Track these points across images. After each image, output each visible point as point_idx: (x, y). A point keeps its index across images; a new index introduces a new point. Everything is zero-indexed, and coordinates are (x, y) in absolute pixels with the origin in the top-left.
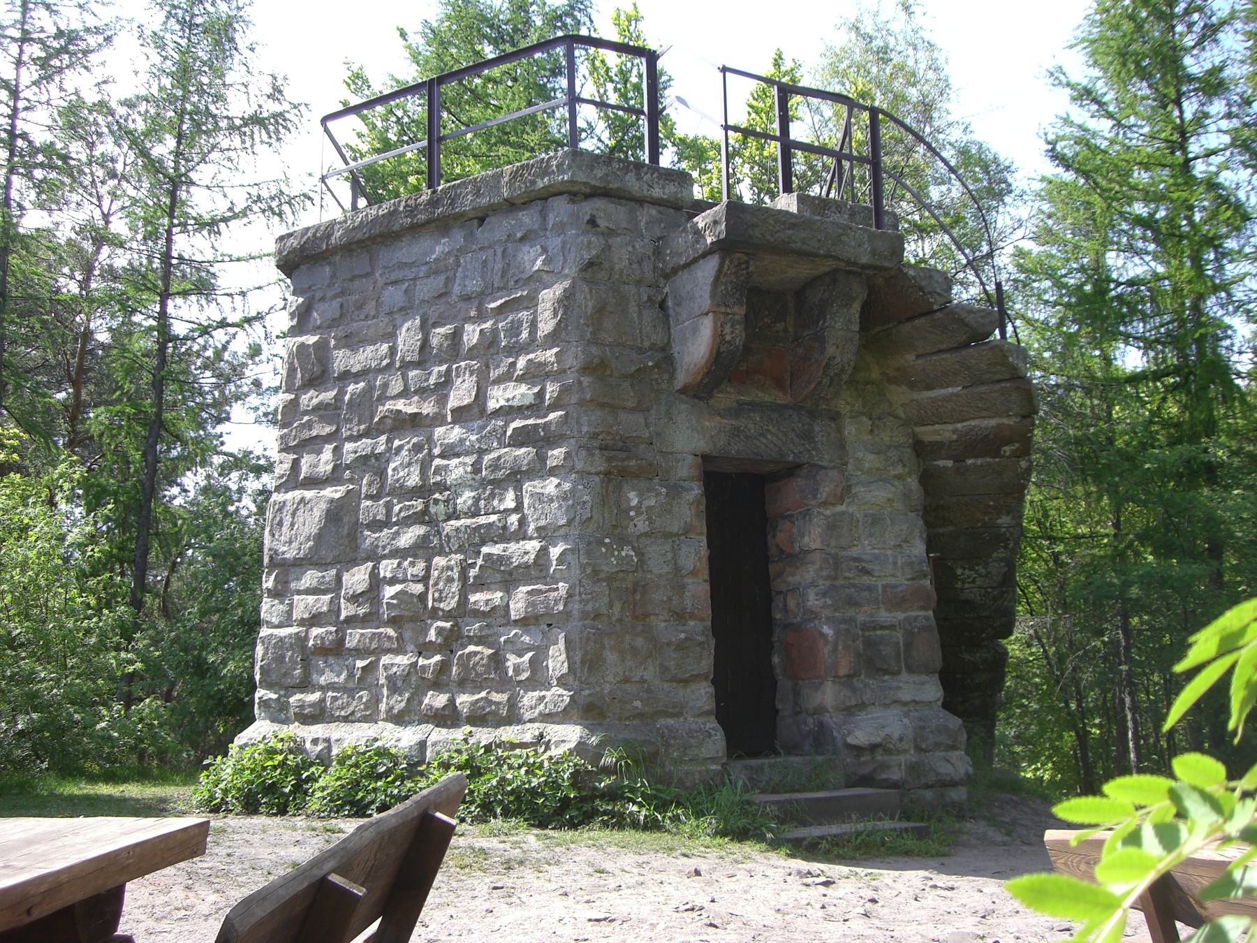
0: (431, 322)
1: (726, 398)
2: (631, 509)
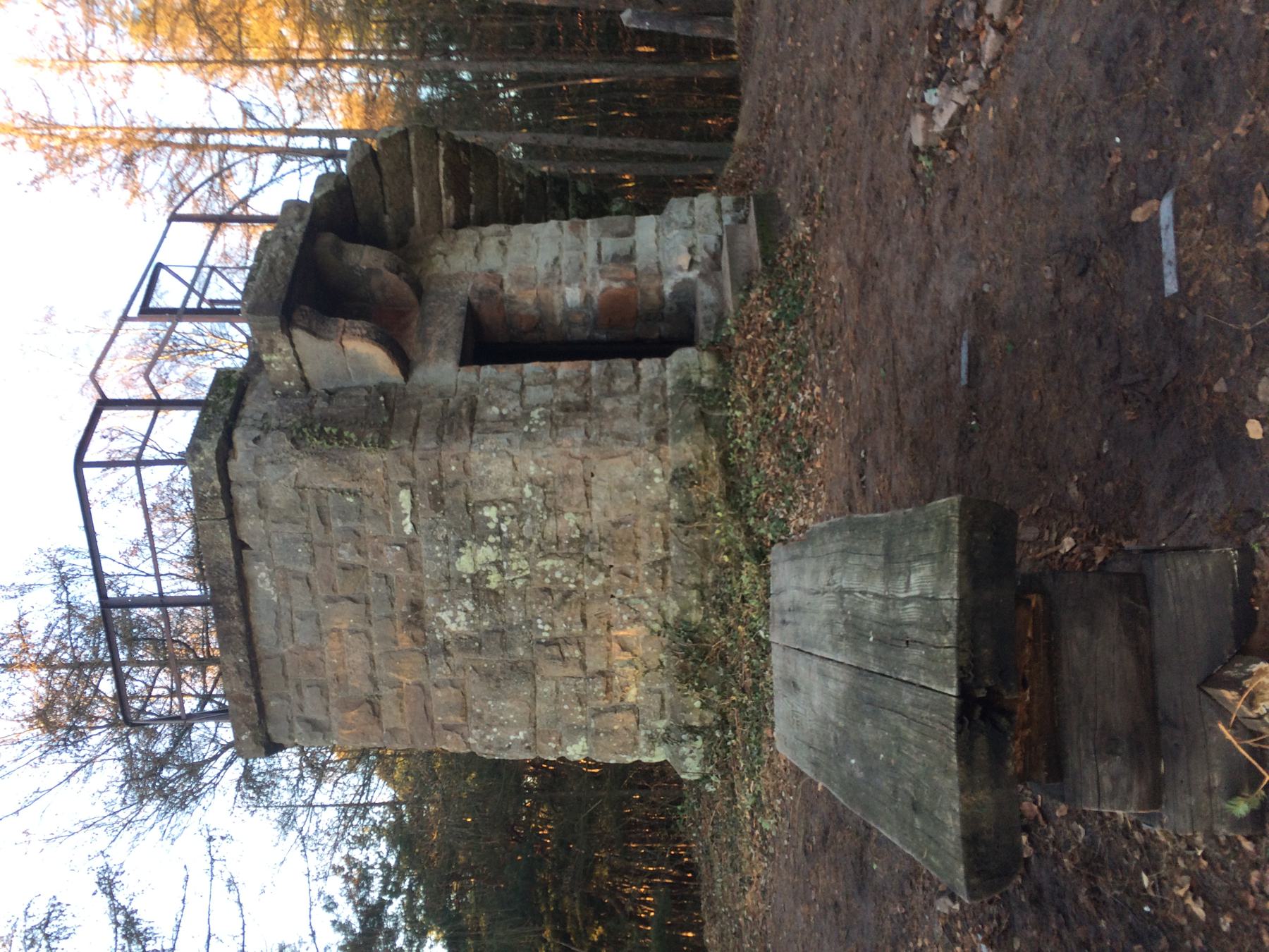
0: (332, 594)
1: (412, 347)
2: (473, 888)
